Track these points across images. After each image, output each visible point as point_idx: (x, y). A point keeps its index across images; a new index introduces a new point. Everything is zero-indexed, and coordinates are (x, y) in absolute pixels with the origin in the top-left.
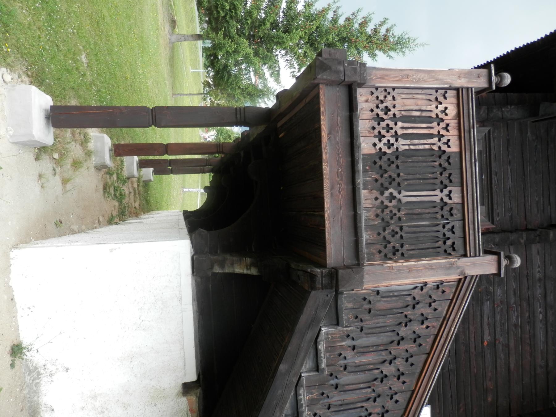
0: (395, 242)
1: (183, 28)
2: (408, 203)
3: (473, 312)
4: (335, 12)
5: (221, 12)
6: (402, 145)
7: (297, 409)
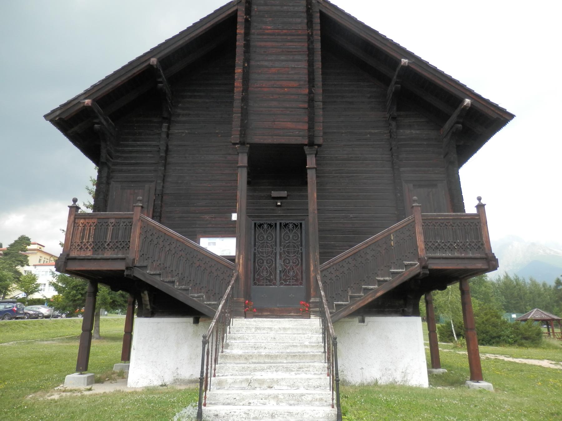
4: (87, 208)
5: (78, 297)
6: (91, 240)
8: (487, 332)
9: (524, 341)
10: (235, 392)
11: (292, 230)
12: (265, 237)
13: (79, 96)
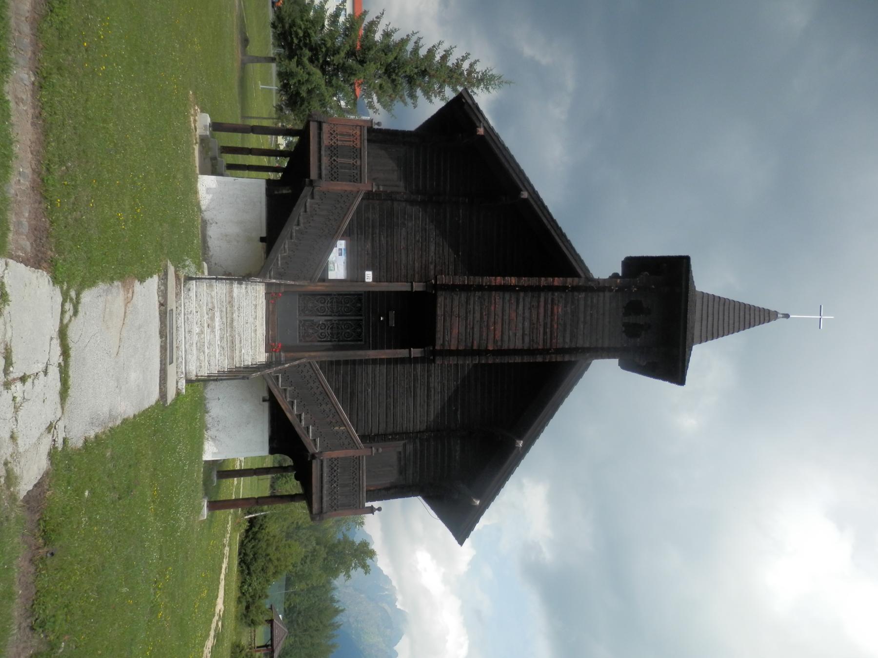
0: (335, 175)
1: (254, 49)
4: (416, 43)
6: (339, 143)
8: (255, 558)
9: (244, 604)
10: (204, 299)
13: (487, 122)
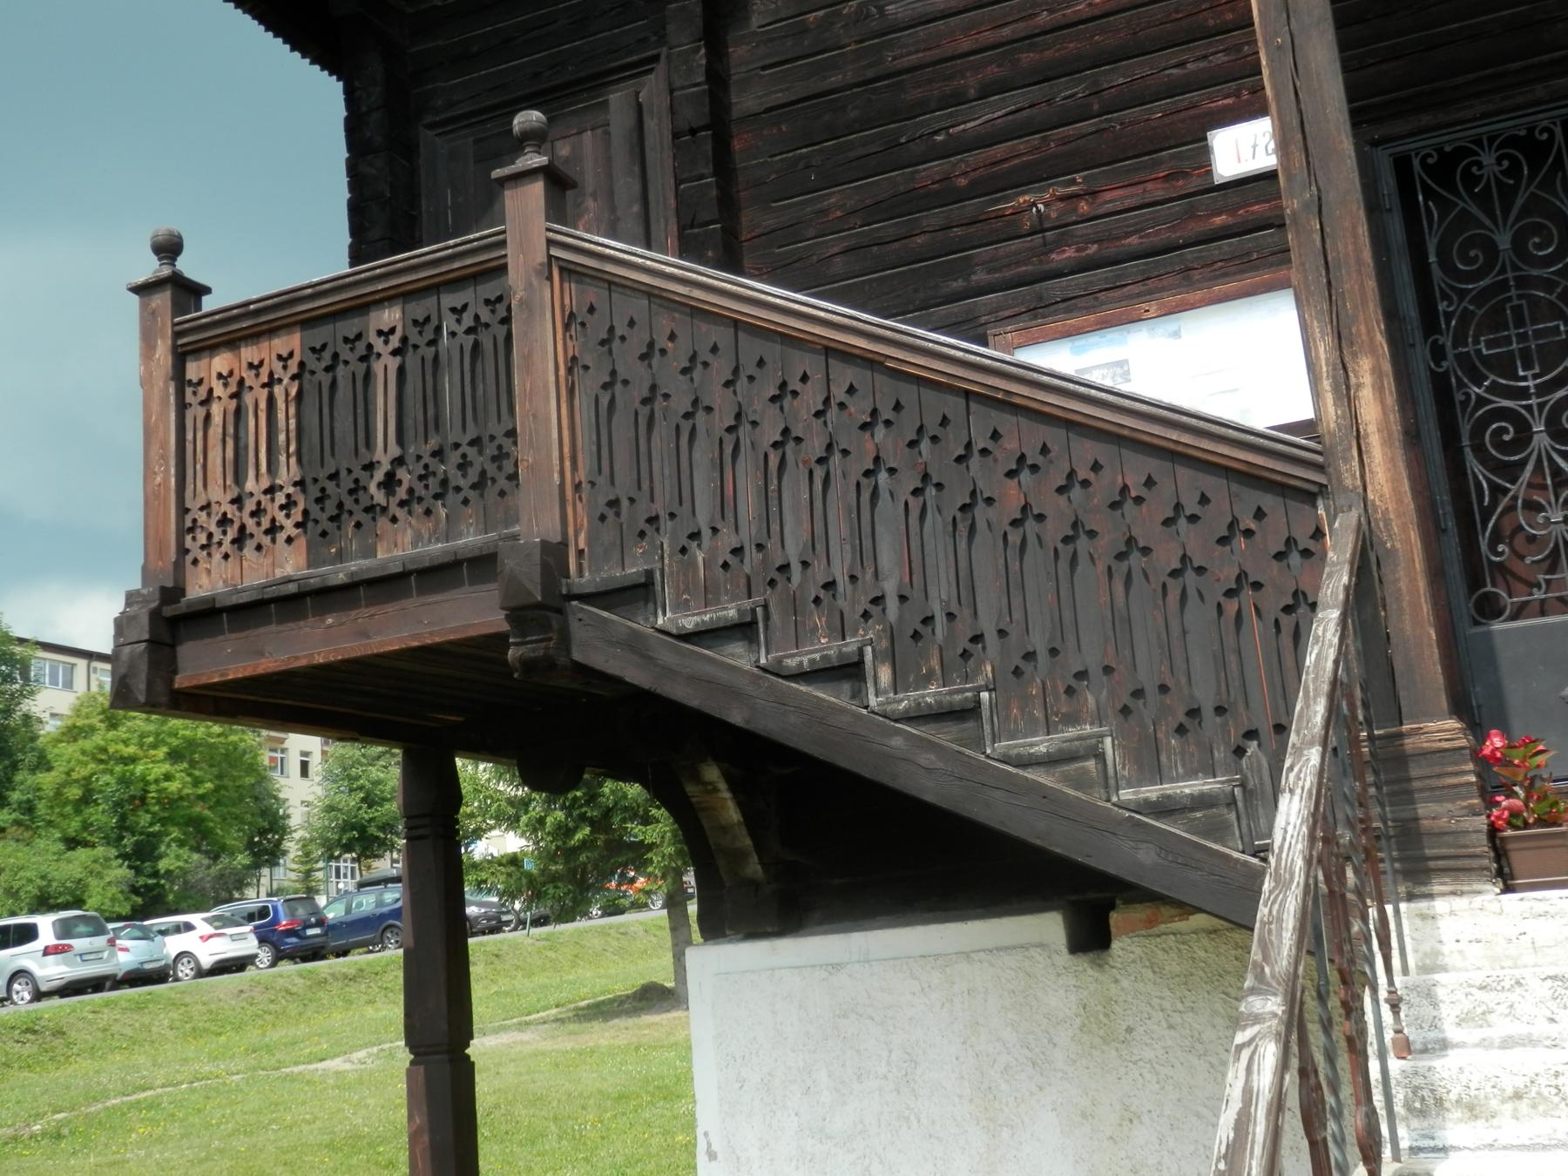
2: (400, 440)
3: (917, 52)
5: (579, 836)
6: (288, 472)
7: (833, 668)
11: (1508, 196)
12: (1504, 241)
